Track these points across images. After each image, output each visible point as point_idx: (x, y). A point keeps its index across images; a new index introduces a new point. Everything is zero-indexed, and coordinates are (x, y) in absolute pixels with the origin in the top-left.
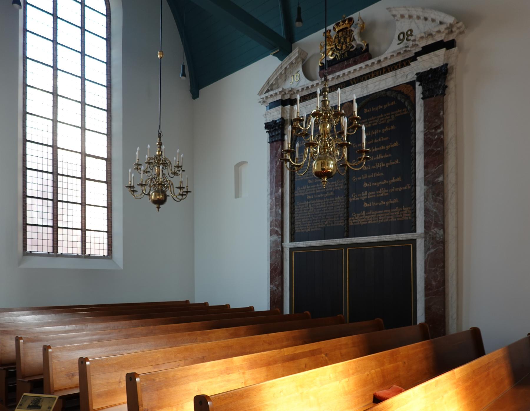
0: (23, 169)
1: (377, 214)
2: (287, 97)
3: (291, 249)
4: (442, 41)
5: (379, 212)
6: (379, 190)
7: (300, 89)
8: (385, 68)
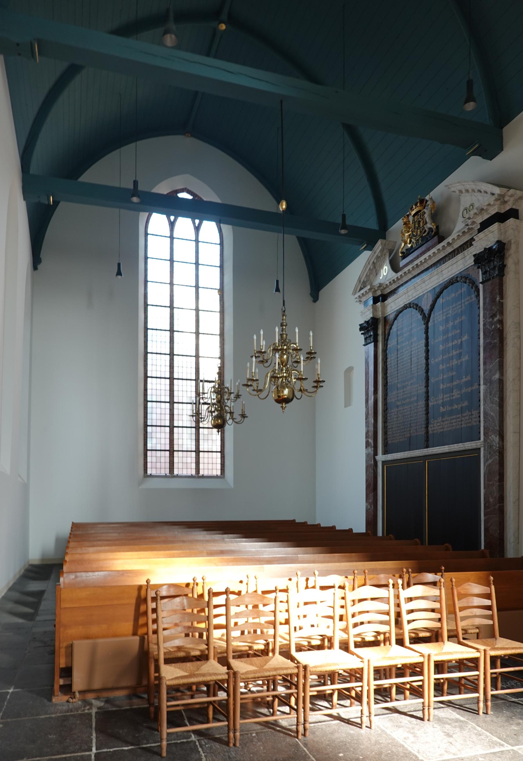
0: (144, 402)
1: (451, 419)
2: (379, 293)
3: (384, 463)
4: (497, 213)
5: (452, 417)
6: (453, 392)
7: (388, 283)
8: (457, 249)
